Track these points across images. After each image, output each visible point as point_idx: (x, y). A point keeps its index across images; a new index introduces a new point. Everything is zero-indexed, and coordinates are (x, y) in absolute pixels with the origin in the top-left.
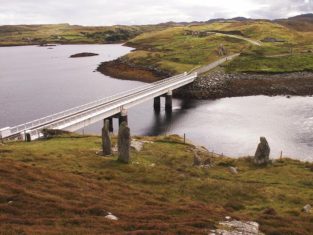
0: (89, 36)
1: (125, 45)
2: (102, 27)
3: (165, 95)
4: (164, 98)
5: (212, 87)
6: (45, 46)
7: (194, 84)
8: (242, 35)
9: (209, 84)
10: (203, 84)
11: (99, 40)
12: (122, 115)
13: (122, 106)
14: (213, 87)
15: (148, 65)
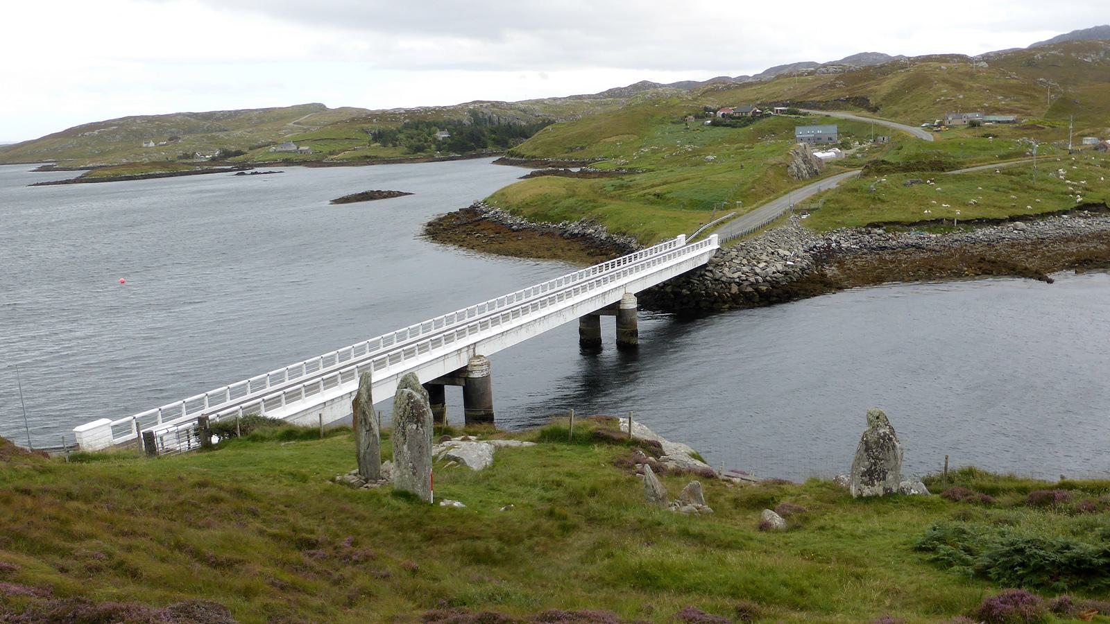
2: (427, 110)
3: (614, 309)
4: (613, 318)
5: (768, 278)
9: (758, 270)
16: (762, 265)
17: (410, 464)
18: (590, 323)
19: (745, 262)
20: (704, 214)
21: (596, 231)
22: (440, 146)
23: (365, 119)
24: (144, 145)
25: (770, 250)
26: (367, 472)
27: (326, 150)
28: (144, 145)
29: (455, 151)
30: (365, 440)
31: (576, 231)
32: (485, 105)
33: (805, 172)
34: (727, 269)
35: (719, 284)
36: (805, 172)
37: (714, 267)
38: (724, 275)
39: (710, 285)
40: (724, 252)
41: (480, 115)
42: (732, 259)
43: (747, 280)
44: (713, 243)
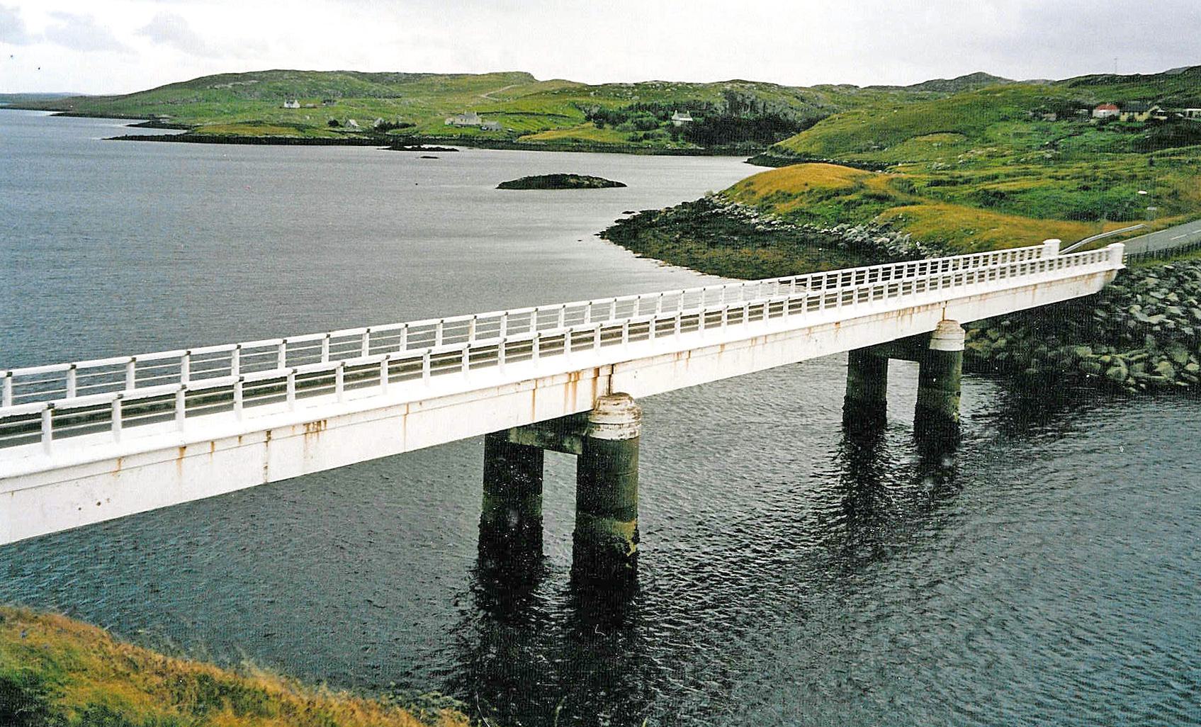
0: (601, 119)
1: (756, 161)
2: (665, 86)
3: (914, 347)
6: (413, 149)
7: (1106, 308)
10: (1161, 311)
11: (646, 137)
12: (598, 434)
13: (605, 372)
15: (847, 221)
19: (1173, 297)
20: (1088, 226)
21: (891, 240)
22: (675, 132)
23: (580, 91)
24: (286, 105)
27: (520, 128)
28: (286, 105)
29: (699, 143)
31: (859, 239)
32: (748, 85)
34: (1138, 307)
37: (1113, 301)
38: (1132, 317)
40: (1133, 277)
41: (739, 99)
42: (1149, 290)
44: (1114, 258)
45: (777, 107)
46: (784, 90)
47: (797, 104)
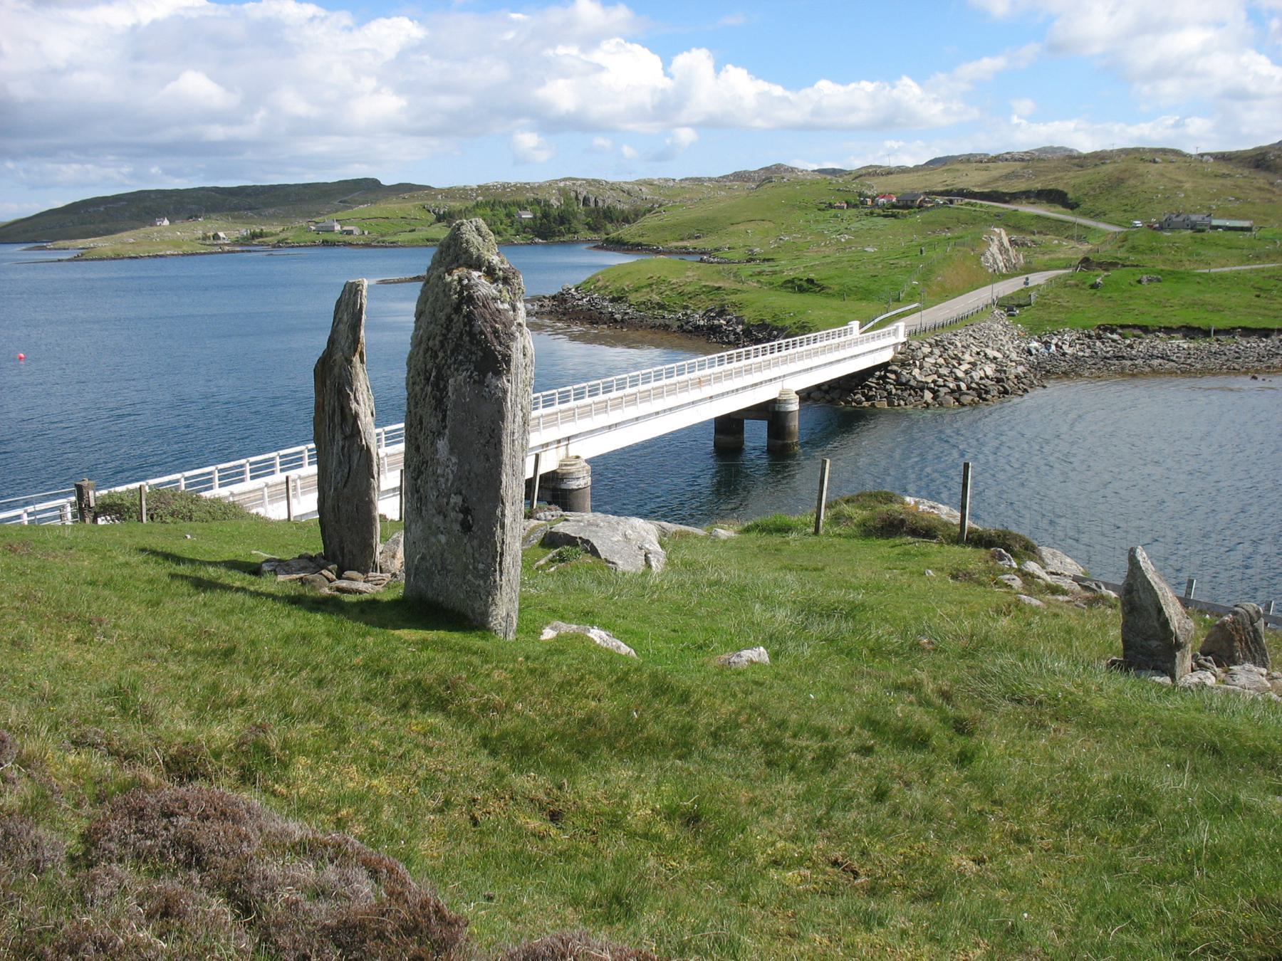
2: (504, 186)
4: (763, 425)
5: (974, 385)
8: (1072, 206)
9: (961, 374)
14: (977, 384)
16: (965, 367)
17: (456, 500)
18: (729, 426)
25: (975, 349)
26: (342, 549)
30: (340, 463)
33: (1001, 264)
35: (906, 390)
36: (1001, 264)
39: (894, 391)
43: (945, 386)
44: (898, 333)
45: (609, 200)
46: (613, 187)
47: (624, 197)
